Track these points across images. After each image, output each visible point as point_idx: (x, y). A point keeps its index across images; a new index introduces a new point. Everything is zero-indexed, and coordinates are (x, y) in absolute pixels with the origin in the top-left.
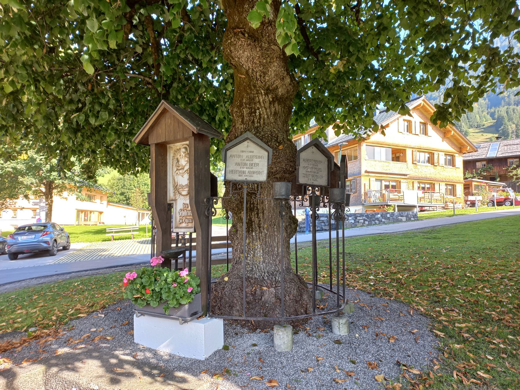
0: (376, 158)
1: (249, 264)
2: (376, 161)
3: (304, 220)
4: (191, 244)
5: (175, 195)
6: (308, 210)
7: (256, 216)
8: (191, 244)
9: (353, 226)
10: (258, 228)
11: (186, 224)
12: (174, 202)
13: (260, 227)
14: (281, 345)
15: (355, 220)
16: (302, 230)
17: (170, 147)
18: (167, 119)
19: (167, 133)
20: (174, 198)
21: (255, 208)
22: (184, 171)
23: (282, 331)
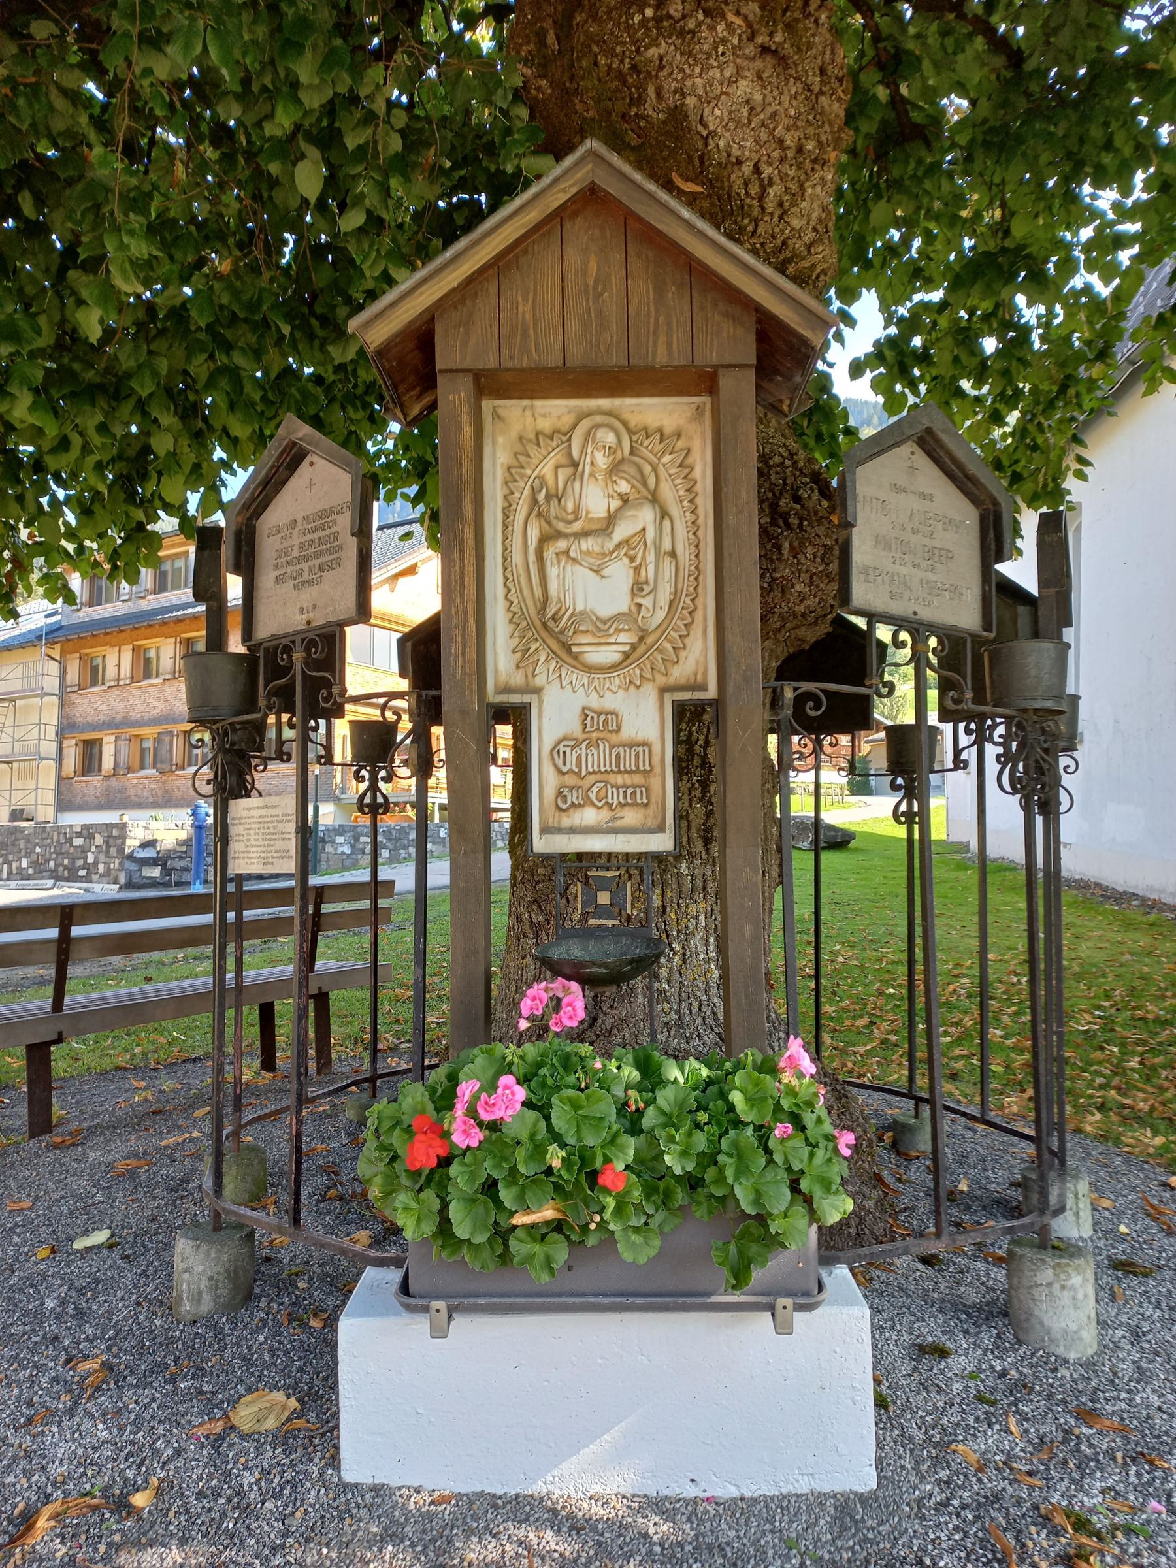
0: (377, 664)
1: (667, 999)
2: (377, 670)
3: (186, 843)
4: (239, 916)
5: (524, 656)
6: (202, 811)
7: (698, 794)
8: (239, 916)
9: (348, 862)
10: (699, 844)
11: (605, 814)
12: (533, 699)
13: (707, 841)
14: (1080, 1328)
15: (353, 847)
16: (175, 878)
17: (496, 416)
18: (571, 253)
19: (573, 329)
20: (518, 679)
21: (697, 761)
22: (610, 546)
23: (1077, 1269)
